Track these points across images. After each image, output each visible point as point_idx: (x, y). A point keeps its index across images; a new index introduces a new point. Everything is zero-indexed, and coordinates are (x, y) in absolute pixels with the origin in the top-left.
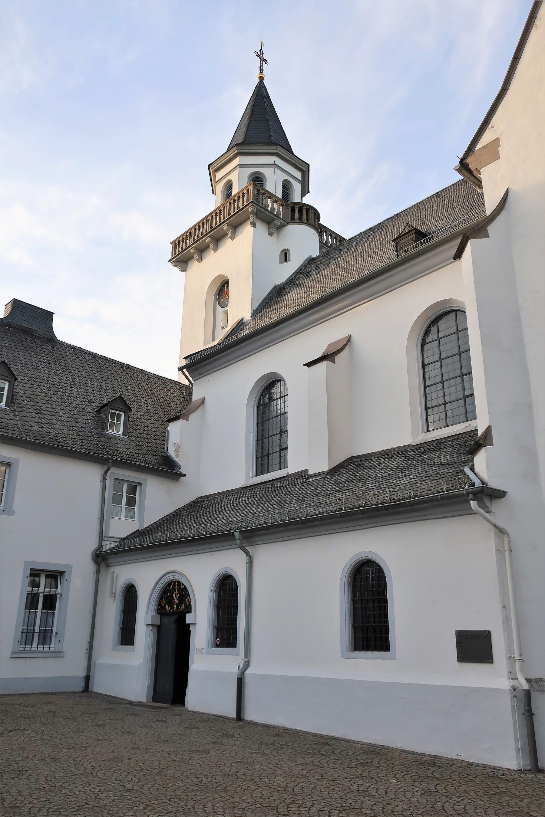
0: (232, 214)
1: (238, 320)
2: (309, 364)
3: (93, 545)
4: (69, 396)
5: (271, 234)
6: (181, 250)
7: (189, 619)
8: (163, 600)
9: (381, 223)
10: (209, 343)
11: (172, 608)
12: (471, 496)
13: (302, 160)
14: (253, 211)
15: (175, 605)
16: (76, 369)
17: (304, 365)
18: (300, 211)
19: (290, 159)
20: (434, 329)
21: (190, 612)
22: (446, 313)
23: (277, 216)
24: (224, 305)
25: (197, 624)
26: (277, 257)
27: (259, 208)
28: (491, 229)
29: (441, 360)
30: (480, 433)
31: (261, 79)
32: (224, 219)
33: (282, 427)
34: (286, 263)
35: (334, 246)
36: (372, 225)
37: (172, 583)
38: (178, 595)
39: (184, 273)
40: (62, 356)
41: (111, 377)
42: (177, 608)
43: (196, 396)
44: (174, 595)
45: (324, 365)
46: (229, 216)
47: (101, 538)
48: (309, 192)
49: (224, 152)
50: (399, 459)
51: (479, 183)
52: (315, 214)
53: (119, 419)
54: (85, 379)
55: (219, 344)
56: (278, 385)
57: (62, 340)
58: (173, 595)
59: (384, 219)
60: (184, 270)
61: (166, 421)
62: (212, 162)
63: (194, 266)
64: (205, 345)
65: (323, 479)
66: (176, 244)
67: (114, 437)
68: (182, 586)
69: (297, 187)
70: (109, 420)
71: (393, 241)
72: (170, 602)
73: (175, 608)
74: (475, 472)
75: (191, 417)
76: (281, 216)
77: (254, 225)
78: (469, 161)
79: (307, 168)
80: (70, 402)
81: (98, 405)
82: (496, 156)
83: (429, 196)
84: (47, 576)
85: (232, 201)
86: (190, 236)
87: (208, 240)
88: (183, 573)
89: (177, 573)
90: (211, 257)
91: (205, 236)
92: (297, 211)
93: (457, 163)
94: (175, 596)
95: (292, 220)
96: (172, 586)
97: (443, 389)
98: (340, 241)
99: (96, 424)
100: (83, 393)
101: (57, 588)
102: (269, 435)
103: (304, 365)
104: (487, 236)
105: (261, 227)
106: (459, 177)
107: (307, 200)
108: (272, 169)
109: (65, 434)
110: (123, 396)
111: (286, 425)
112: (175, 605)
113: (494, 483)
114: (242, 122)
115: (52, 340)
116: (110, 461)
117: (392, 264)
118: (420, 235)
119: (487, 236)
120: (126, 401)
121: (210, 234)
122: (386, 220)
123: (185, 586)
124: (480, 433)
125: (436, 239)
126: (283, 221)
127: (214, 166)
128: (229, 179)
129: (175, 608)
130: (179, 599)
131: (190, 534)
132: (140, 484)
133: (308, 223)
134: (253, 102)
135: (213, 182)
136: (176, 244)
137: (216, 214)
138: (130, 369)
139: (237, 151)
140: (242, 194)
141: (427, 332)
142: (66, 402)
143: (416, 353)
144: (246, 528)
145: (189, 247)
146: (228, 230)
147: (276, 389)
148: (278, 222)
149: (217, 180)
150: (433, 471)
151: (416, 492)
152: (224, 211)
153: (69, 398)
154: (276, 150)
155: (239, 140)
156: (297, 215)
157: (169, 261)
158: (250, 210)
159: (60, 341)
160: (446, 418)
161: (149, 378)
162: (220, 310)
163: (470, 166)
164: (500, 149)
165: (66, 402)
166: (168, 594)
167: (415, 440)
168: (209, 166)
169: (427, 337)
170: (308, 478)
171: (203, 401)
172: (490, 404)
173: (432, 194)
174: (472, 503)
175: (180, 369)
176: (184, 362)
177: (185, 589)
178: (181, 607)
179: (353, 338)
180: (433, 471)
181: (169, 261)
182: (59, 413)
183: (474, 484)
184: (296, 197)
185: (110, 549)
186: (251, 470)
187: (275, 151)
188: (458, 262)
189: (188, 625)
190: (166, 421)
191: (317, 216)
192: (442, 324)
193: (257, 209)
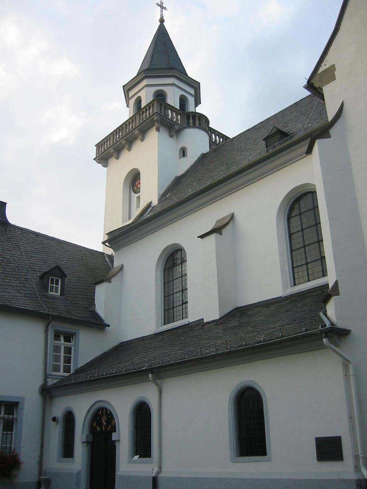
0: (141, 122)
1: (148, 204)
2: (202, 237)
3: (39, 382)
4: (19, 267)
5: (171, 136)
6: (103, 150)
7: (114, 437)
8: (95, 422)
9: (255, 126)
10: (126, 221)
11: (102, 429)
12: (323, 335)
13: (195, 79)
14: (157, 119)
15: (104, 426)
16: (24, 246)
17: (198, 237)
18: (194, 119)
19: (185, 79)
20: (297, 206)
21: (115, 431)
22: (305, 194)
23: (176, 123)
24: (137, 191)
25: (121, 441)
26: (177, 153)
27: (162, 117)
28: (332, 131)
29: (302, 230)
30: (330, 286)
31: (162, 21)
32: (135, 126)
33: (183, 286)
34: (184, 158)
35: (221, 144)
36: (249, 128)
37: (100, 409)
38: (106, 419)
39: (106, 168)
40: (13, 236)
41: (51, 251)
42: (105, 428)
43: (117, 264)
44: (103, 419)
45: (213, 237)
46: (139, 123)
47: (46, 376)
48: (200, 103)
49: (135, 76)
50: (273, 307)
51: (322, 97)
52: (205, 120)
53: (57, 284)
54: (31, 253)
55: (133, 223)
56: (179, 253)
57: (13, 223)
58: (102, 419)
59: (258, 123)
60: (105, 166)
61: (94, 284)
62: (125, 84)
63: (113, 162)
64: (123, 223)
65: (215, 326)
66: (99, 146)
67: (53, 298)
68: (108, 412)
69: (191, 100)
70: (50, 285)
71: (264, 140)
72: (100, 424)
73: (104, 429)
74: (327, 316)
75: (113, 280)
76: (179, 122)
77: (158, 130)
78: (313, 81)
79: (198, 86)
80: (19, 272)
81: (41, 273)
82: (333, 78)
83: (291, 104)
84: (5, 405)
85: (141, 113)
86: (110, 140)
87: (124, 142)
88: (118, 413)
89: (105, 402)
90: (126, 155)
91: (121, 139)
92: (191, 118)
93: (305, 83)
94: (104, 419)
95: (188, 126)
96: (101, 412)
97: (305, 253)
98: (226, 140)
99: (40, 287)
100: (29, 264)
101: (13, 414)
102: (173, 292)
103: (198, 237)
104: (329, 136)
105: (164, 133)
106: (308, 93)
107: (199, 110)
108: (171, 87)
109: (16, 296)
110: (59, 265)
111: (186, 284)
112: (104, 426)
113: (341, 324)
114: (148, 53)
115: (6, 223)
116: (51, 316)
117: (262, 158)
118: (283, 135)
119: (329, 136)
120: (63, 270)
121: (125, 138)
122: (259, 123)
123: (110, 412)
124: (330, 286)
125: (296, 138)
126: (181, 126)
127: (127, 86)
128: (139, 96)
129: (104, 429)
130: (106, 421)
131: (114, 371)
132: (75, 334)
133: (200, 127)
134: (156, 39)
135: (127, 99)
136: (98, 146)
137: (129, 122)
138: (65, 244)
139: (144, 75)
140: (149, 105)
141: (292, 209)
142: (16, 272)
143: (283, 225)
144: (155, 365)
145: (109, 149)
146: (138, 134)
147: (178, 255)
148: (177, 127)
149: (130, 97)
150: (285, 318)
151: (283, 334)
152: (135, 120)
153: (19, 268)
154: (174, 73)
155: (146, 67)
156: (191, 121)
157: (94, 159)
158: (155, 119)
159: (11, 224)
160: (308, 275)
161: (80, 250)
162: (135, 196)
163: (315, 85)
164: (335, 72)
165: (16, 272)
166: (98, 418)
167: (286, 293)
168: (123, 86)
169: (292, 213)
170: (204, 325)
171: (122, 268)
172: (336, 264)
173: (293, 103)
174: (324, 340)
175: (104, 243)
176: (106, 238)
177: (111, 414)
178: (108, 428)
179: (235, 215)
180: (285, 318)
181: (94, 159)
182: (11, 280)
183: (325, 326)
184: (191, 108)
185: (53, 385)
186: (160, 319)
187: (173, 74)
188: (309, 156)
189: (114, 442)
190: (94, 284)
191: (207, 121)
192: (302, 203)
193: (160, 118)
